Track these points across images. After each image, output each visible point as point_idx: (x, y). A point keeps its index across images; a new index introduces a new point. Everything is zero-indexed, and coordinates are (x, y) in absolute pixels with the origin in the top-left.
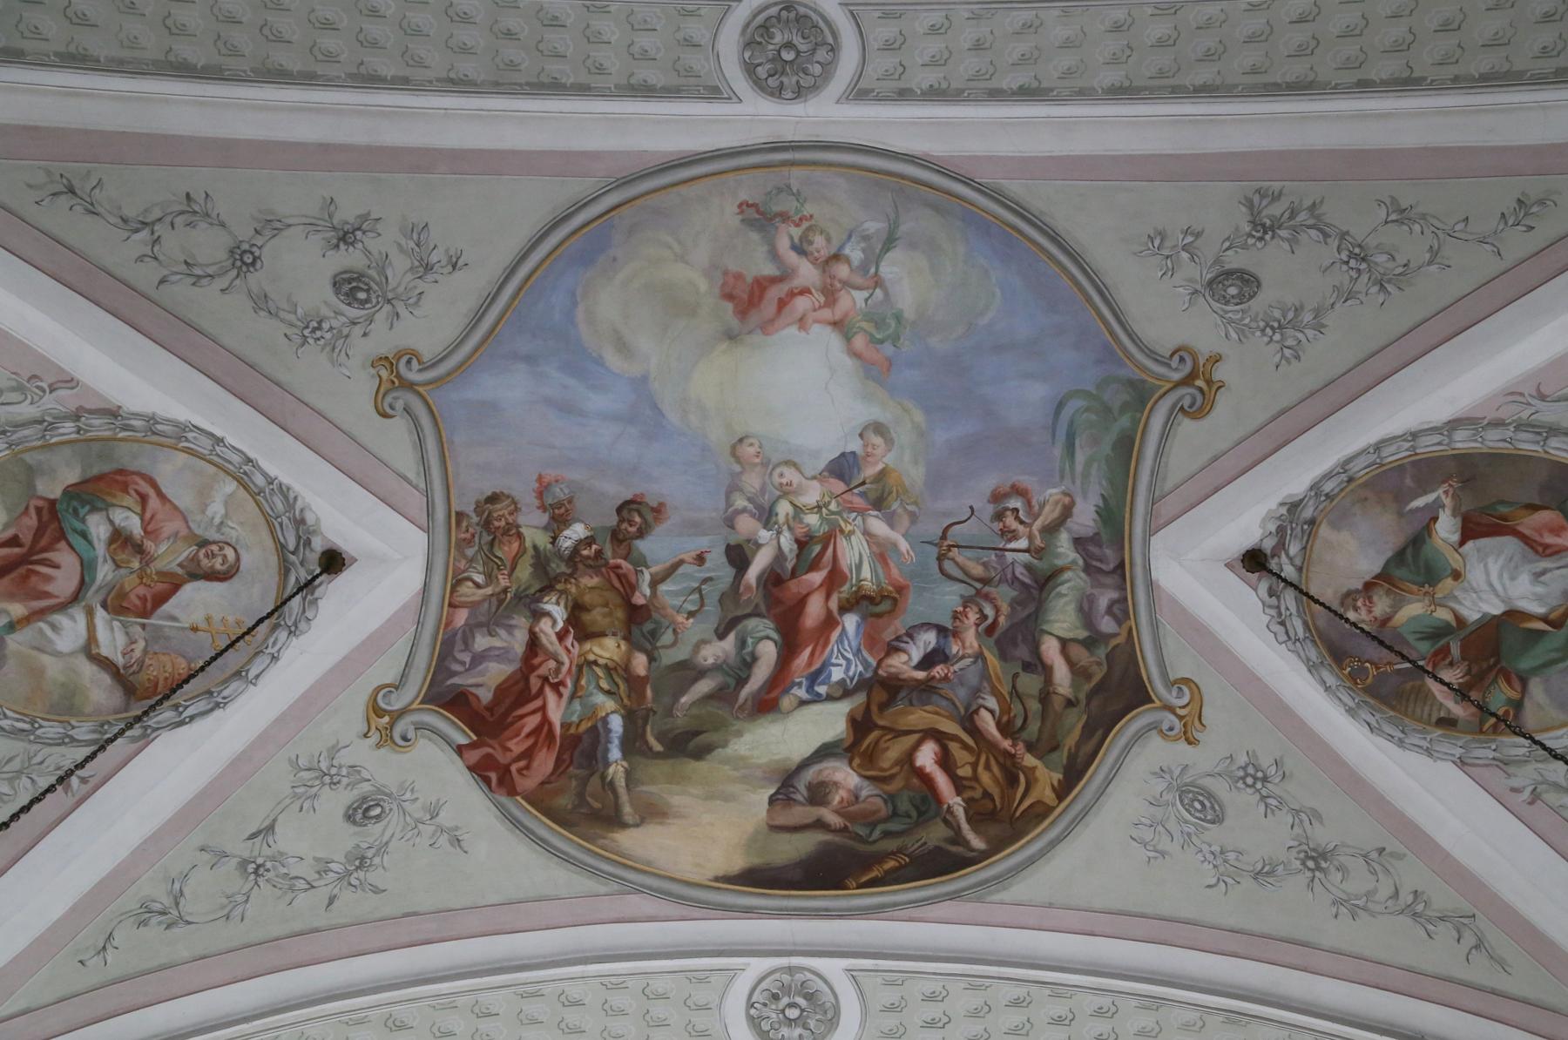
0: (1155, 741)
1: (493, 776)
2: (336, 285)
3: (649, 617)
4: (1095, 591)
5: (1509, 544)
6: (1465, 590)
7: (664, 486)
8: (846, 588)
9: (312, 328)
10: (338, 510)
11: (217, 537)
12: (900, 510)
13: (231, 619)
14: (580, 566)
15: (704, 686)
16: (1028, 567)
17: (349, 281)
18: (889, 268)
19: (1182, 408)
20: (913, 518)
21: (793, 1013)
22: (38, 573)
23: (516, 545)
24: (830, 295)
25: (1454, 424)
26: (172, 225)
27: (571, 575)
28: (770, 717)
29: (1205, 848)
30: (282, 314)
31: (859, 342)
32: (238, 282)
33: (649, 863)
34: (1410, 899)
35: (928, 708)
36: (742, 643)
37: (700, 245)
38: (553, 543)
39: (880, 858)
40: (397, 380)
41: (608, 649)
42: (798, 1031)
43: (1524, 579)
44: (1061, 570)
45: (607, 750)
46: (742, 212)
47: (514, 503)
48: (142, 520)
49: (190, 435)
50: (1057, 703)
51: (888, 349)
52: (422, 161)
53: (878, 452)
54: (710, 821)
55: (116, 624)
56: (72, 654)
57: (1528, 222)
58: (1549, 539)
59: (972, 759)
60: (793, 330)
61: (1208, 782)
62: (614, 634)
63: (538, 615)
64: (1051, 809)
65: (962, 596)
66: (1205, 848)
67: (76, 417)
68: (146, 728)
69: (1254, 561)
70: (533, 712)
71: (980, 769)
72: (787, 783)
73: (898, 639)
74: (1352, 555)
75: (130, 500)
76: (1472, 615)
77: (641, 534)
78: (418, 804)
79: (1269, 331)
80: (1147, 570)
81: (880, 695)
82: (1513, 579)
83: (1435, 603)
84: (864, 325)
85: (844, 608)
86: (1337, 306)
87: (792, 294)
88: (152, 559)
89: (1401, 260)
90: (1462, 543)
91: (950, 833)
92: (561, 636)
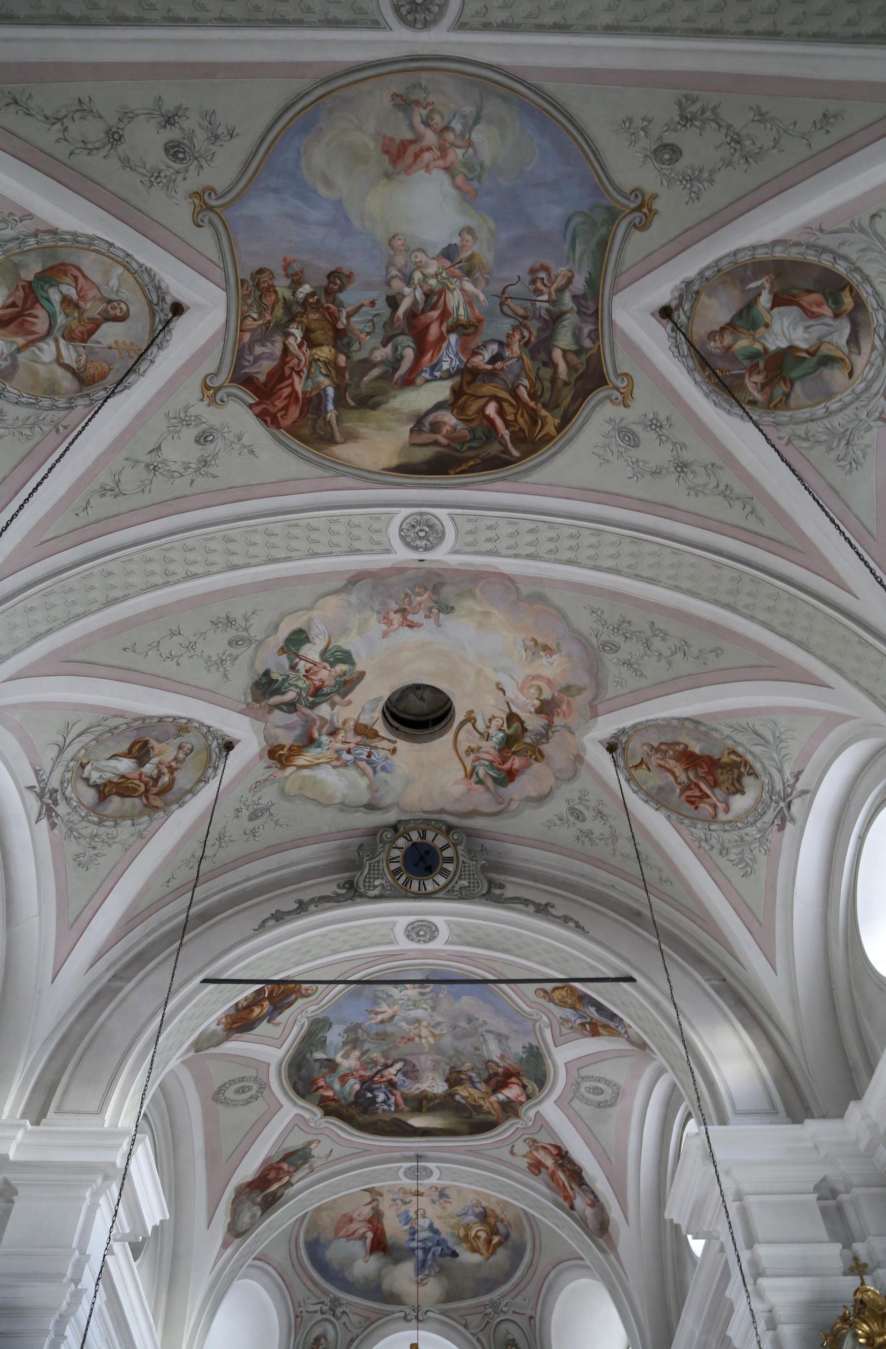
0: (608, 406)
1: (268, 419)
2: (166, 150)
3: (346, 335)
4: (583, 325)
5: (794, 310)
6: (770, 334)
7: (351, 263)
8: (450, 320)
9: (155, 176)
10: (179, 281)
11: (117, 298)
12: (480, 277)
13: (128, 342)
14: (308, 308)
15: (376, 372)
16: (548, 310)
17: (173, 147)
18: (477, 136)
19: (634, 225)
20: (487, 282)
21: (422, 534)
22: (27, 321)
23: (273, 297)
24: (443, 151)
25: (775, 243)
26: (73, 118)
27: (304, 313)
28: (411, 388)
29: (629, 459)
30: (139, 169)
31: (459, 180)
32: (112, 151)
33: (349, 462)
34: (724, 488)
35: (493, 384)
36: (395, 349)
37: (370, 119)
38: (293, 296)
39: (466, 460)
40: (205, 205)
41: (325, 352)
42: (425, 542)
43: (800, 329)
44: (565, 313)
45: (326, 406)
46: (393, 100)
47: (272, 273)
48: (76, 288)
49: (96, 242)
50: (559, 384)
51: (475, 184)
52: (208, 71)
53: (470, 244)
54: (380, 441)
55: (70, 346)
56: (51, 363)
57: (828, 128)
58: (815, 309)
59: (514, 411)
60: (422, 172)
61: (634, 427)
62: (328, 345)
63: (287, 335)
64: (554, 438)
65: (512, 326)
66: (629, 459)
67: (36, 235)
68: (92, 400)
69: (666, 313)
70: (288, 386)
71: (519, 416)
72: (419, 422)
73: (478, 348)
74: (717, 311)
75: (69, 280)
76: (772, 347)
77: (341, 290)
78: (232, 434)
79: (684, 182)
80: (610, 315)
81: (468, 378)
82: (794, 329)
83: (755, 340)
84: (462, 170)
85: (450, 331)
86: (722, 170)
87: (422, 151)
88: (85, 311)
89: (758, 144)
90: (772, 308)
91: (501, 448)
92: (300, 346)
